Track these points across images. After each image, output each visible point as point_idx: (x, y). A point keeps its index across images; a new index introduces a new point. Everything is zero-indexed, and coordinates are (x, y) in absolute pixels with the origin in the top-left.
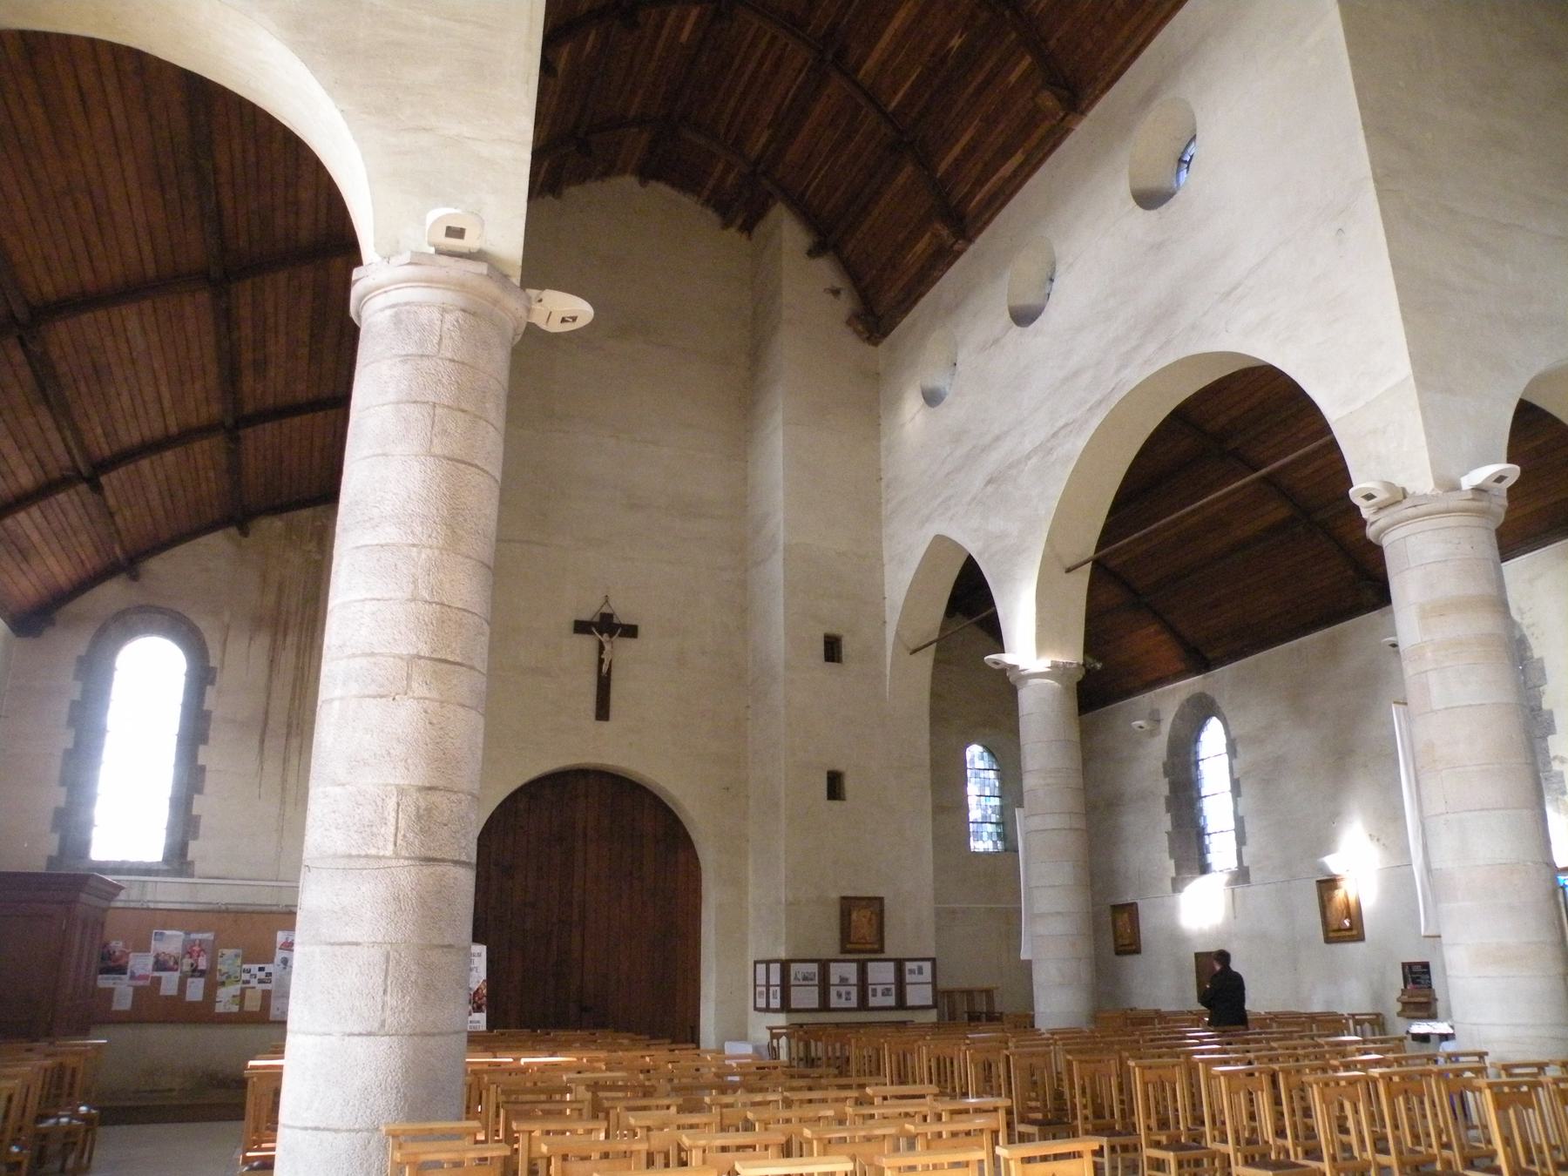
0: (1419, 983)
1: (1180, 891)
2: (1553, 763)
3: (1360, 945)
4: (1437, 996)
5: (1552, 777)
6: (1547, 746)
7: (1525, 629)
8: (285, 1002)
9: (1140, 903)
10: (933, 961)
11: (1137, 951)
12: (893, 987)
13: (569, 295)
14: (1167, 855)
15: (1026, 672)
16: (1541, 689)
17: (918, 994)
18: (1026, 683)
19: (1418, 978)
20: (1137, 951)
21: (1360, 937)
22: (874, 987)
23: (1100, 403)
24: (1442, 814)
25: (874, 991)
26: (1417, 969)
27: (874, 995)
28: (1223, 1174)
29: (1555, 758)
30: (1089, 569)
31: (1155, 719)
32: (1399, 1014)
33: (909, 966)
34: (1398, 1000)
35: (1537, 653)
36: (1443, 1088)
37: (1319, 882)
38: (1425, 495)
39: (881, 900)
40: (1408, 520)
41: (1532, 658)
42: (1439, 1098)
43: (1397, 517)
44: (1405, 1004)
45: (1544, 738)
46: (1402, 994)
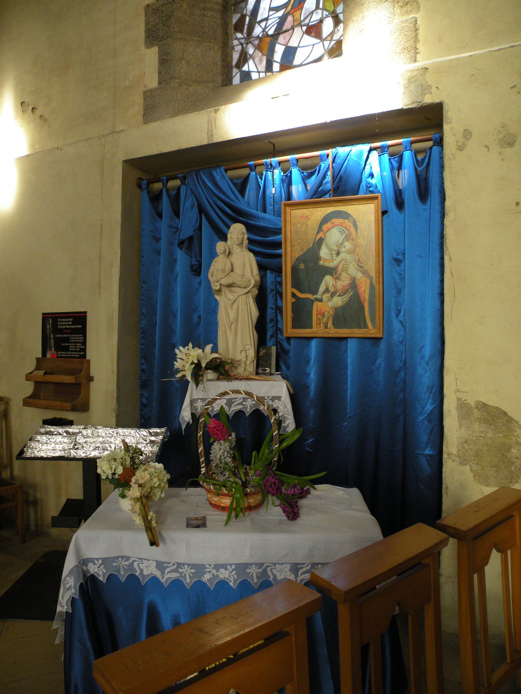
0: (67, 349)
19: (67, 340)
26: (65, 324)
32: (27, 402)
34: (28, 377)
36: (205, 180)
42: (205, 183)
44: (38, 384)
46: (38, 368)
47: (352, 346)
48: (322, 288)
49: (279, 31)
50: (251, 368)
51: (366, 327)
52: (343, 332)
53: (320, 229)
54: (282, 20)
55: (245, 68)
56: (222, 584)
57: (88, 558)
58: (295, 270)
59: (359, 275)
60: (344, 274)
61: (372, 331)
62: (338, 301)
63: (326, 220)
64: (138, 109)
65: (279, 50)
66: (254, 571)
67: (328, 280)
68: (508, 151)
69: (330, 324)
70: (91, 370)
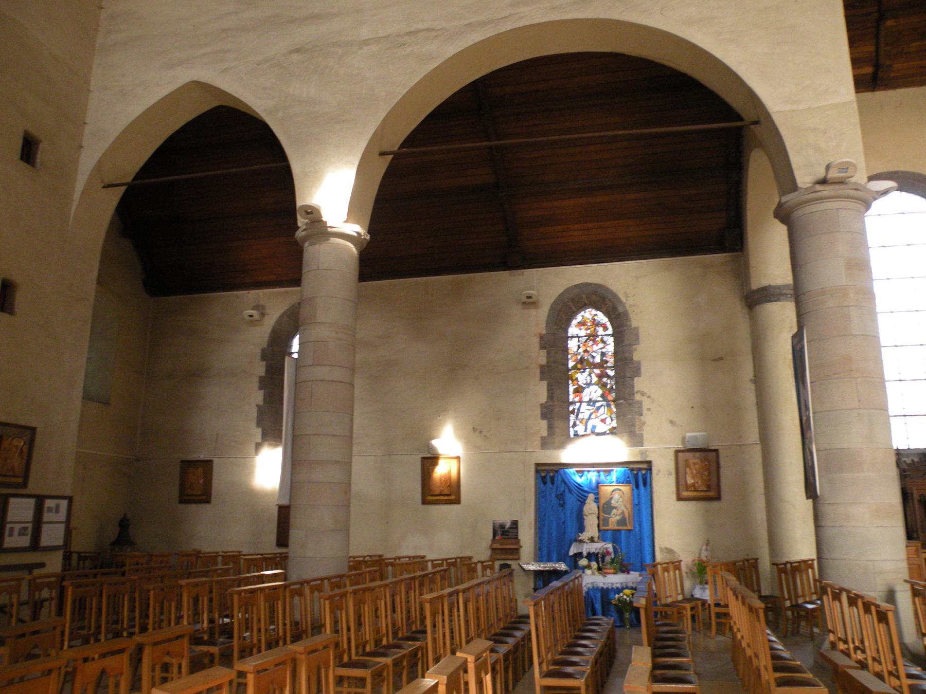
0: (508, 535)
1: (257, 455)
2: (636, 395)
3: (455, 507)
5: (635, 403)
6: (633, 384)
9: (216, 461)
10: (70, 499)
11: (208, 501)
12: (30, 526)
14: (253, 424)
15: (333, 230)
16: (634, 347)
17: (52, 535)
18: (328, 240)
20: (208, 501)
21: (457, 501)
22: (12, 525)
23: (484, 24)
25: (12, 529)
27: (11, 535)
28: (231, 691)
29: (638, 392)
30: (389, 161)
31: (262, 311)
33: (49, 503)
35: (634, 324)
37: (423, 458)
39: (33, 430)
40: (848, 198)
41: (631, 326)
43: (841, 192)
45: (632, 378)
47: (623, 532)
48: (612, 513)
49: (589, 419)
51: (627, 526)
53: (611, 495)
56: (617, 588)
59: (625, 509)
60: (620, 509)
61: (629, 527)
62: (618, 518)
63: (614, 491)
64: (538, 442)
66: (624, 584)
67: (614, 511)
68: (670, 476)
69: (615, 525)
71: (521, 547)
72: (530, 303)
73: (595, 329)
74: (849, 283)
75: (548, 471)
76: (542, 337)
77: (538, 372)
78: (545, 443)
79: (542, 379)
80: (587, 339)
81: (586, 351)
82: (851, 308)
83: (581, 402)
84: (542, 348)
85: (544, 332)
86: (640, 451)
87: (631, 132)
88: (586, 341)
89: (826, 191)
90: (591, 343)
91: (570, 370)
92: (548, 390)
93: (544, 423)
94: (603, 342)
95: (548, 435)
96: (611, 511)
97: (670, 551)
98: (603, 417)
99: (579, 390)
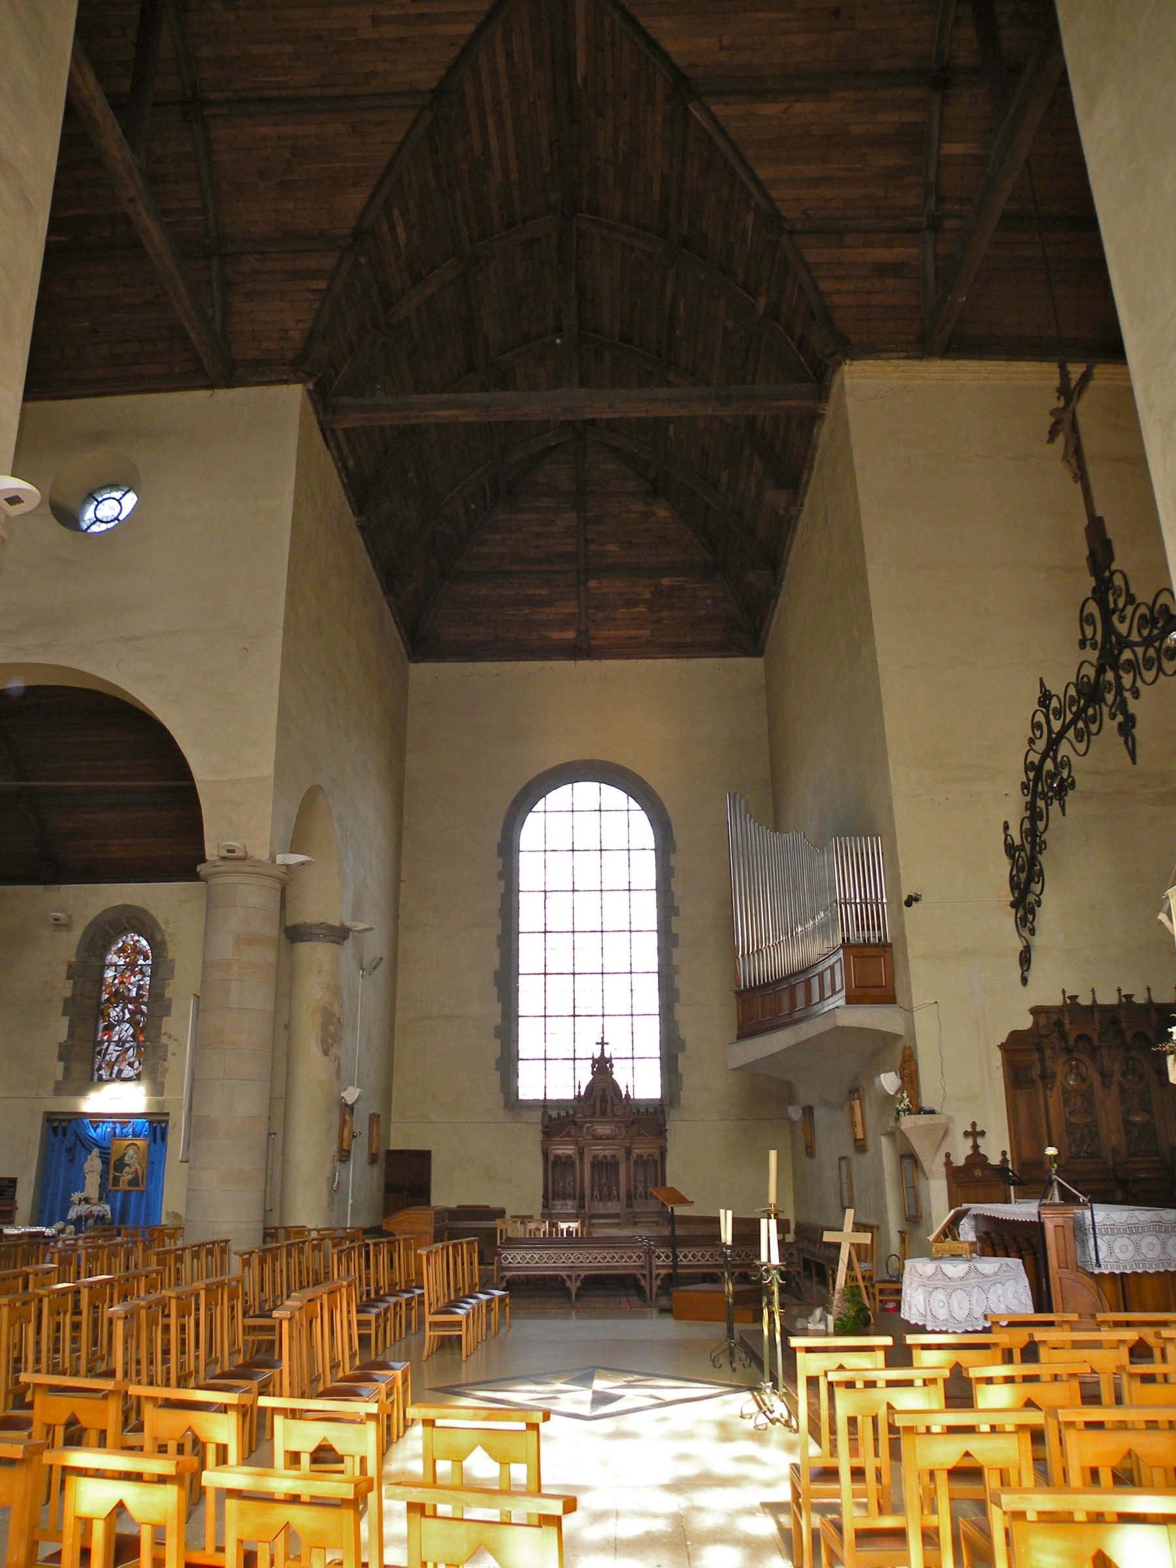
2: (162, 1037)
4: (18, 1206)
7: (166, 936)
8: (834, 1266)
13: (26, 369)
16: (167, 982)
24: (220, 1079)
38: (261, 861)
43: (238, 869)
45: (160, 1018)
48: (124, 1171)
50: (96, 1200)
51: (139, 1186)
52: (131, 1188)
53: (125, 1149)
54: (118, 1057)
55: (100, 1072)
57: (867, 631)
58: (115, 1163)
59: (139, 1167)
61: (141, 1188)
62: (130, 1177)
64: (51, 1087)
65: (116, 1069)
67: (127, 1169)
70: (855, 1025)
71: (17, 1208)
72: (61, 925)
73: (135, 958)
74: (235, 958)
75: (61, 1121)
76: (70, 966)
77: (61, 1005)
78: (58, 1089)
79: (64, 1014)
80: (125, 969)
81: (122, 982)
82: (232, 982)
83: (109, 1041)
84: (69, 978)
85: (74, 960)
86: (158, 1101)
87: (88, 784)
88: (123, 971)
89: (226, 866)
90: (129, 973)
91: (102, 1004)
92: (70, 1027)
93: (60, 1065)
94: (141, 972)
95: (64, 1079)
96: (123, 1169)
97: (176, 1216)
98: (132, 1060)
99: (109, 1028)
